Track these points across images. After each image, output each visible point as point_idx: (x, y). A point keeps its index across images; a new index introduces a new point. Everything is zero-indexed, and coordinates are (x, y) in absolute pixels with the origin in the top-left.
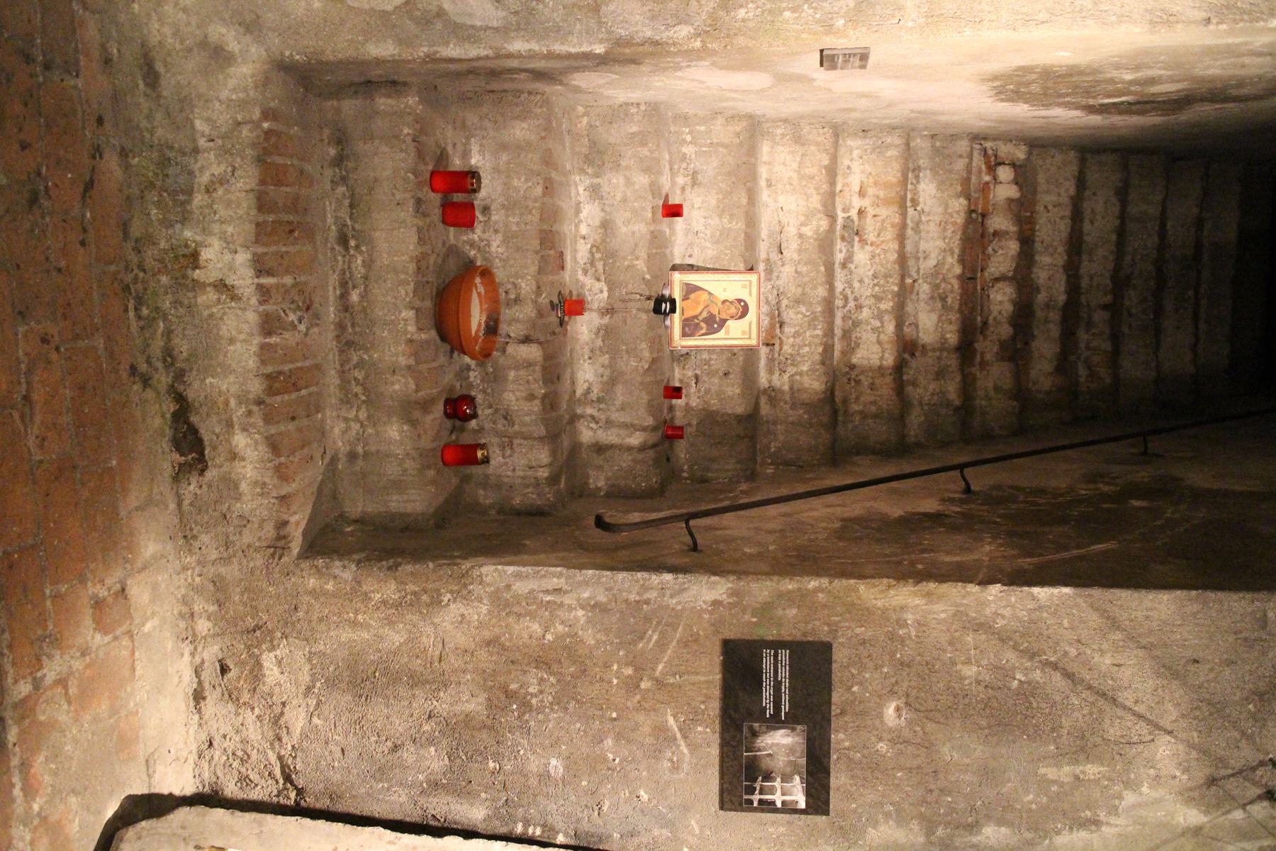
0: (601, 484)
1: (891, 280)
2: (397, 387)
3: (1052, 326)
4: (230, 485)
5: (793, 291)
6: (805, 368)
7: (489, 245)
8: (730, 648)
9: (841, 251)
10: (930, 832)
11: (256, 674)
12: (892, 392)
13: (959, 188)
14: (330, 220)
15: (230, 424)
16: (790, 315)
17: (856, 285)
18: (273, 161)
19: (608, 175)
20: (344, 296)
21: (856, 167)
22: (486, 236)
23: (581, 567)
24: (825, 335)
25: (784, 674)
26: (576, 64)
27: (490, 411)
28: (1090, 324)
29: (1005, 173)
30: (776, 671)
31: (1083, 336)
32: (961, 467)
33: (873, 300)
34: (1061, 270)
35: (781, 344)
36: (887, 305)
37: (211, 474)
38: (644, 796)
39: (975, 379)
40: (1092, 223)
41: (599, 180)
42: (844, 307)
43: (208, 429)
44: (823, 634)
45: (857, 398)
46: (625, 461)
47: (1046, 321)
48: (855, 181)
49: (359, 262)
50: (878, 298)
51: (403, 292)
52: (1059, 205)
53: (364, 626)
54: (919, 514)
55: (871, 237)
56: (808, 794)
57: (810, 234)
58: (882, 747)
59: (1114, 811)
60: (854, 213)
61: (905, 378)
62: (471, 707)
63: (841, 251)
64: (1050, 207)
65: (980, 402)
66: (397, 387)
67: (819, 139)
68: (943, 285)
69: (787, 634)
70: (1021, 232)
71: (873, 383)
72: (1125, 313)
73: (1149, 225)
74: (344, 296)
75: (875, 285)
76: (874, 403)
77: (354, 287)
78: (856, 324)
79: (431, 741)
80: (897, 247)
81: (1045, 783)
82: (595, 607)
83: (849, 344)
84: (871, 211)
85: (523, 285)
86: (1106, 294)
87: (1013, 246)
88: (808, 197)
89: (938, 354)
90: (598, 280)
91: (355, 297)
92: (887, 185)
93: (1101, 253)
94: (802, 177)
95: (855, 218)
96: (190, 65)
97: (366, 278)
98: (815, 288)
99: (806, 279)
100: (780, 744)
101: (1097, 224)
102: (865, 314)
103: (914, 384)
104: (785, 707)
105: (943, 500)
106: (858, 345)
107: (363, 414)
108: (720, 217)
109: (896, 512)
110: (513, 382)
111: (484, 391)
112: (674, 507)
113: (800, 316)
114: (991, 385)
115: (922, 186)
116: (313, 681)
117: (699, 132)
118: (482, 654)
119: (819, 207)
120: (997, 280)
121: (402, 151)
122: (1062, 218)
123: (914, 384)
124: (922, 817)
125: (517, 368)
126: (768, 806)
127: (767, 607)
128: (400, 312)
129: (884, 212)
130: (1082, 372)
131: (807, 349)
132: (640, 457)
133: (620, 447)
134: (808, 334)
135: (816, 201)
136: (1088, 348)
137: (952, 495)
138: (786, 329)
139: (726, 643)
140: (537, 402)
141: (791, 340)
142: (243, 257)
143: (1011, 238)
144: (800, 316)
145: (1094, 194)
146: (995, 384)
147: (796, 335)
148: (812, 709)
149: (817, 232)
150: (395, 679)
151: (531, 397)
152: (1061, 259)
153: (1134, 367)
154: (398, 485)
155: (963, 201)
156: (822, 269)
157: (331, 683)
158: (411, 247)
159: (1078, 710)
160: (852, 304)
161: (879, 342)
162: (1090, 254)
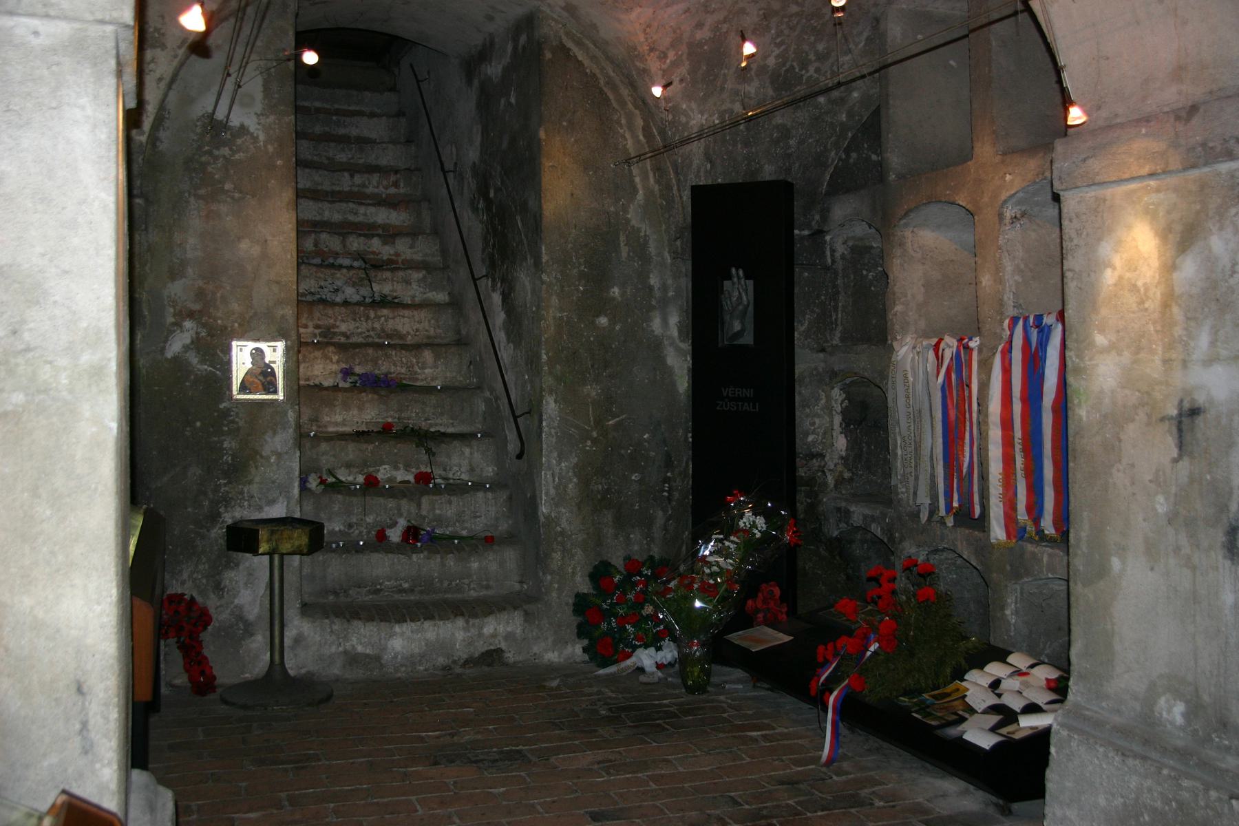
4: (509, 637)
28: (364, 186)
37: (503, 646)
46: (477, 456)
47: (365, 215)
55: (332, 321)
59: (639, 230)
60: (317, 331)
78: (383, 330)
79: (628, 538)
91: (406, 586)
93: (317, 178)
97: (396, 580)
102: (377, 325)
103: (413, 297)
109: (502, 316)
120: (344, 246)
123: (413, 297)
125: (434, 509)
129: (317, 314)
135: (318, 354)
147: (395, 365)
151: (450, 502)
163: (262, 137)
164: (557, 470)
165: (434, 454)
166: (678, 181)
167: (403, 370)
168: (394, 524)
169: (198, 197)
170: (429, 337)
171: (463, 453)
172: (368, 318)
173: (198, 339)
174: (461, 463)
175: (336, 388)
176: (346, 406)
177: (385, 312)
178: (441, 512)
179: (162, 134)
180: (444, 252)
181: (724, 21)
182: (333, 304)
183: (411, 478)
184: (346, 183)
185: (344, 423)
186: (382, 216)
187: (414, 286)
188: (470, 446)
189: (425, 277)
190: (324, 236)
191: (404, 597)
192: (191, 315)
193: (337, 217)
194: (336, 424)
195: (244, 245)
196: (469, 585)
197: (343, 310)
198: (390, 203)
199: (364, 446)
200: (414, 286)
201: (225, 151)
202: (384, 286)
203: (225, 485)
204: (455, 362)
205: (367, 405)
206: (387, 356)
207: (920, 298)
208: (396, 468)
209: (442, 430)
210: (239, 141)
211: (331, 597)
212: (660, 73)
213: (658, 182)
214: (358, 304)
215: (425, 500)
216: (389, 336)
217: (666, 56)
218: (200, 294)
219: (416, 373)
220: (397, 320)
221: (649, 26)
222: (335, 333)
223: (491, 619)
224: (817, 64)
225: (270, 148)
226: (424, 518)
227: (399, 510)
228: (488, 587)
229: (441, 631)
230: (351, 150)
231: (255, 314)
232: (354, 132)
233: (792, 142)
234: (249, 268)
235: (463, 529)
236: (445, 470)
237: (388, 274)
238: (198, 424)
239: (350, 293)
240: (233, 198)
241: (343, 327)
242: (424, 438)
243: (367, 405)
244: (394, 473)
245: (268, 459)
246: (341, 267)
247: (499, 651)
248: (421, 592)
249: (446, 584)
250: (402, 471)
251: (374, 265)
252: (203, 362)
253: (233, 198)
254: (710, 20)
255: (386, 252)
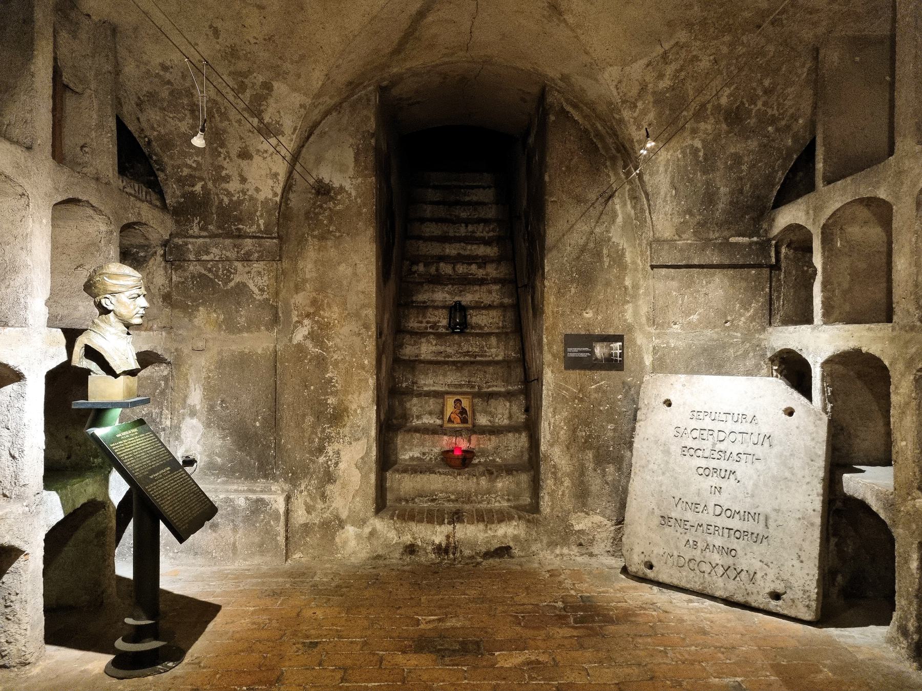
4: (516, 538)
5: (456, 347)
8: (567, 368)
10: (628, 302)
11: (581, 532)
15: (494, 536)
16: (465, 349)
18: (408, 516)
20: (453, 501)
23: (818, 586)
25: (576, 350)
26: (481, 273)
28: (473, 232)
30: (574, 352)
31: (478, 234)
37: (511, 544)
38: (620, 397)
43: (496, 545)
44: (561, 337)
47: (471, 250)
53: (563, 492)
56: (617, 341)
58: (599, 318)
62: (591, 456)
65: (502, 276)
69: (562, 349)
74: (453, 501)
79: (604, 470)
81: (610, 266)
82: (554, 412)
91: (453, 497)
96: (375, 543)
97: (446, 493)
100: (599, 351)
104: (587, 349)
107: (493, 496)
116: (583, 511)
118: (572, 451)
124: (623, 305)
126: (622, 355)
127: (554, 356)
130: (491, 234)
133: (510, 410)
139: (566, 368)
142: (438, 528)
148: (589, 340)
150: (582, 482)
151: (490, 440)
153: (491, 213)
154: (518, 484)
157: (584, 505)
159: (587, 257)
163: (354, 194)
164: (552, 421)
166: (649, 206)
169: (314, 237)
173: (313, 332)
179: (291, 196)
181: (681, 70)
184: (462, 231)
186: (482, 250)
190: (442, 264)
192: (308, 315)
193: (454, 252)
194: (429, 385)
195: (342, 268)
201: (331, 204)
203: (328, 428)
206: (468, 341)
207: (846, 286)
210: (339, 197)
212: (632, 120)
213: (634, 208)
217: (636, 107)
218: (314, 302)
221: (620, 82)
223: (503, 525)
224: (764, 99)
225: (359, 201)
229: (468, 532)
231: (349, 314)
232: (475, 199)
233: (744, 167)
234: (345, 283)
237: (477, 288)
238: (312, 388)
240: (334, 236)
245: (355, 411)
247: (508, 548)
252: (315, 347)
253: (334, 236)
254: (670, 70)
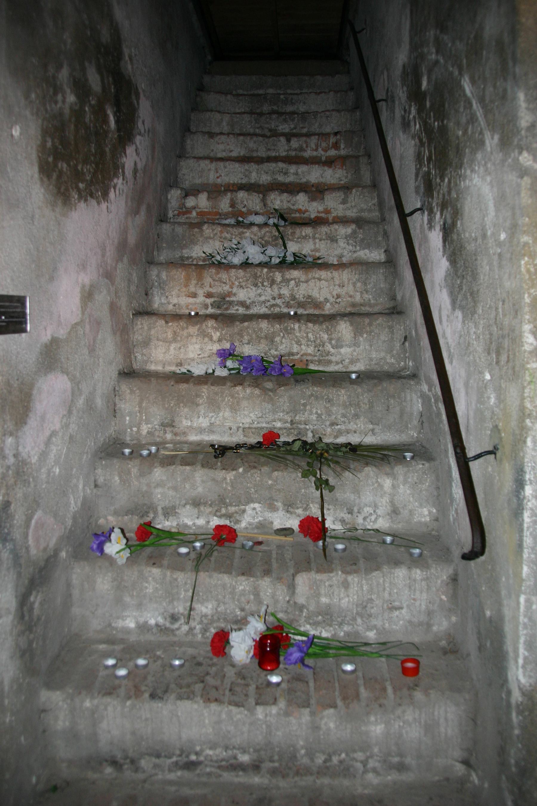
0: (425, 511)
1: (259, 274)
2: (332, 725)
3: (300, 171)
6: (326, 336)
7: (206, 616)
9: (237, 310)
12: (346, 271)
13: (196, 230)
14: (172, 776)
17: (263, 298)
19: (155, 500)
21: (175, 301)
22: (198, 619)
24: (299, 321)
27: (359, 621)
28: (301, 149)
29: (190, 202)
31: (308, 154)
32: (403, 217)
33: (275, 286)
34: (261, 166)
35: (306, 354)
36: (278, 276)
39: (337, 217)
40: (231, 151)
41: (159, 509)
42: (280, 307)
45: (351, 296)
48: (184, 301)
49: (211, 752)
50: (273, 282)
51: (239, 716)
52: (216, 169)
54: (444, 246)
55: (227, 288)
57: (218, 334)
60: (209, 301)
61: (336, 263)
63: (237, 310)
64: (218, 175)
66: (332, 725)
67: (146, 328)
68: (266, 238)
70: (232, 191)
71: (339, 286)
72: (294, 131)
73: (235, 120)
75: (263, 285)
76: (354, 285)
77: (235, 758)
80: (234, 270)
83: (309, 303)
84: (207, 289)
85: (241, 588)
86: (280, 141)
87: (241, 195)
88: (190, 336)
89: (317, 241)
90: (244, 511)
91: (245, 758)
92: (188, 279)
93: (251, 145)
94: (175, 340)
95: (212, 300)
97: (226, 748)
98: (261, 329)
99: (254, 336)
101: (232, 148)
102: (285, 291)
103: (341, 257)
105: (431, 227)
106: (309, 297)
108: (198, 405)
110: (331, 599)
111: (340, 624)
112: (446, 451)
113: (284, 340)
114: (341, 206)
115: (194, 255)
117: (130, 421)
119: (197, 327)
120: (265, 205)
121: (106, 709)
122: (225, 167)
123: (341, 257)
125: (318, 595)
128: (259, 719)
129: (208, 280)
131: (310, 335)
132: (401, 478)
134: (298, 334)
135: (193, 330)
136: (316, 150)
137: (426, 221)
138: (295, 351)
140: (350, 578)
141: (303, 347)
143: (236, 196)
144: (284, 340)
145: (212, 151)
146: (341, 203)
147: (299, 343)
149: (216, 329)
151: (346, 585)
152: (253, 166)
155: (205, 227)
156: (246, 324)
158: (196, 706)
160: (278, 301)
161: (307, 282)
162: (253, 151)
165: (332, 489)
167: (310, 350)
168: (241, 623)
170: (354, 305)
171: (381, 486)
172: (273, 282)
174: (376, 501)
175: (208, 378)
176: (214, 405)
177: (296, 273)
178: (335, 602)
180: (381, 204)
182: (230, 266)
183: (294, 523)
185: (211, 429)
187: (342, 243)
188: (394, 477)
189: (354, 232)
191: (241, 778)
194: (201, 430)
196: (365, 763)
197: (241, 273)
198: (329, 163)
199: (220, 474)
200: (342, 243)
202: (303, 244)
204: (383, 337)
205: (245, 403)
206: (288, 332)
208: (273, 508)
209: (355, 439)
211: (109, 770)
214: (261, 265)
215: (303, 581)
216: (301, 305)
219: (328, 353)
220: (311, 283)
222: (231, 303)
226: (301, 608)
227: (257, 595)
228: (401, 767)
230: (293, 120)
235: (369, 629)
236: (350, 512)
239: (254, 253)
241: (242, 295)
242: (317, 458)
243: (245, 403)
244: (269, 515)
246: (252, 224)
248: (274, 772)
249: (320, 759)
250: (281, 513)
251: (289, 220)
255: (314, 209)
